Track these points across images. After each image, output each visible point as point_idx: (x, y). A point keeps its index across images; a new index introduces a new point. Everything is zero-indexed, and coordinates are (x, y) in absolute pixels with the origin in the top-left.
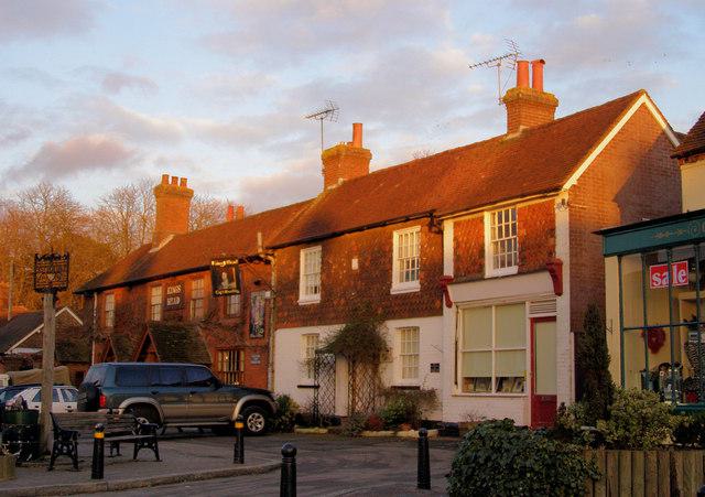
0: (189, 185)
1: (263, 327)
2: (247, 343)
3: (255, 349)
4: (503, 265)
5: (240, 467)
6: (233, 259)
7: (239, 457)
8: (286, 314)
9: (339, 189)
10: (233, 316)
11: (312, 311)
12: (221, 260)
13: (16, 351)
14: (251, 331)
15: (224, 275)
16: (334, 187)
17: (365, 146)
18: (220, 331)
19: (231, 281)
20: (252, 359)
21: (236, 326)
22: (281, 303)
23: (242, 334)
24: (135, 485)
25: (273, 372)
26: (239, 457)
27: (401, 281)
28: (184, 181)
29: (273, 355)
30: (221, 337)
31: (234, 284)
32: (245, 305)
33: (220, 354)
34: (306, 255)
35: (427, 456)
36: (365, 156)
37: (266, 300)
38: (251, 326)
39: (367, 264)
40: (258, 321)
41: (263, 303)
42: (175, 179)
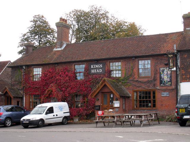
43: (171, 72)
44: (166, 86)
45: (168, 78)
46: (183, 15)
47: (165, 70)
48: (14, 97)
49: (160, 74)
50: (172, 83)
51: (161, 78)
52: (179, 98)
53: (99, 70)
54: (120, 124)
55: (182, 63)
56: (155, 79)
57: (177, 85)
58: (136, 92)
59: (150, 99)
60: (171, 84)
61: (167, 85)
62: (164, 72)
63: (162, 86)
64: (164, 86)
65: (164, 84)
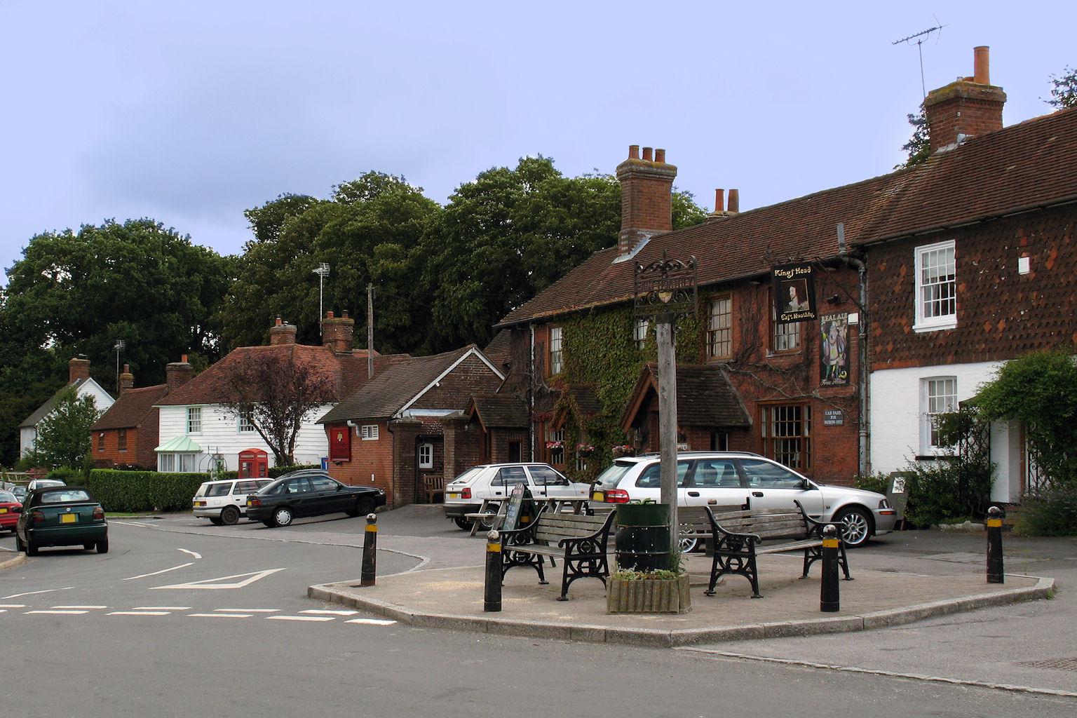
0: (669, 160)
1: (846, 367)
2: (816, 394)
3: (831, 403)
4: (937, 313)
5: (997, 592)
6: (804, 266)
7: (995, 573)
8: (890, 347)
9: (959, 148)
10: (789, 354)
11: (941, 341)
12: (787, 268)
13: (406, 414)
14: (822, 376)
15: (793, 290)
16: (951, 147)
17: (994, 81)
18: (764, 375)
19: (393, 361)
20: (828, 418)
21: (797, 366)
22: (878, 332)
23: (807, 379)
24: (898, 619)
25: (868, 436)
26: (995, 573)
27: (927, 314)
28: (660, 154)
29: (868, 410)
30: (766, 384)
31: (806, 305)
32: (811, 337)
33: (764, 412)
34: (925, 256)
35: (1001, 564)
36: (993, 101)
37: (850, 327)
38: (823, 367)
39: (1049, 265)
40: (835, 356)
41: (843, 333)
42: (647, 151)
43: (849, 329)
44: (835, 385)
45: (841, 355)
46: (40, 232)
47: (834, 324)
48: (249, 384)
49: (822, 341)
50: (852, 376)
51: (822, 354)
52: (281, 469)
53: (624, 240)
54: (318, 487)
55: (874, 297)
56: (808, 362)
57: (861, 379)
58: (767, 407)
59: (800, 419)
60: (848, 379)
61: (836, 381)
62: (832, 333)
63: (825, 386)
64: (831, 386)
65: (830, 379)
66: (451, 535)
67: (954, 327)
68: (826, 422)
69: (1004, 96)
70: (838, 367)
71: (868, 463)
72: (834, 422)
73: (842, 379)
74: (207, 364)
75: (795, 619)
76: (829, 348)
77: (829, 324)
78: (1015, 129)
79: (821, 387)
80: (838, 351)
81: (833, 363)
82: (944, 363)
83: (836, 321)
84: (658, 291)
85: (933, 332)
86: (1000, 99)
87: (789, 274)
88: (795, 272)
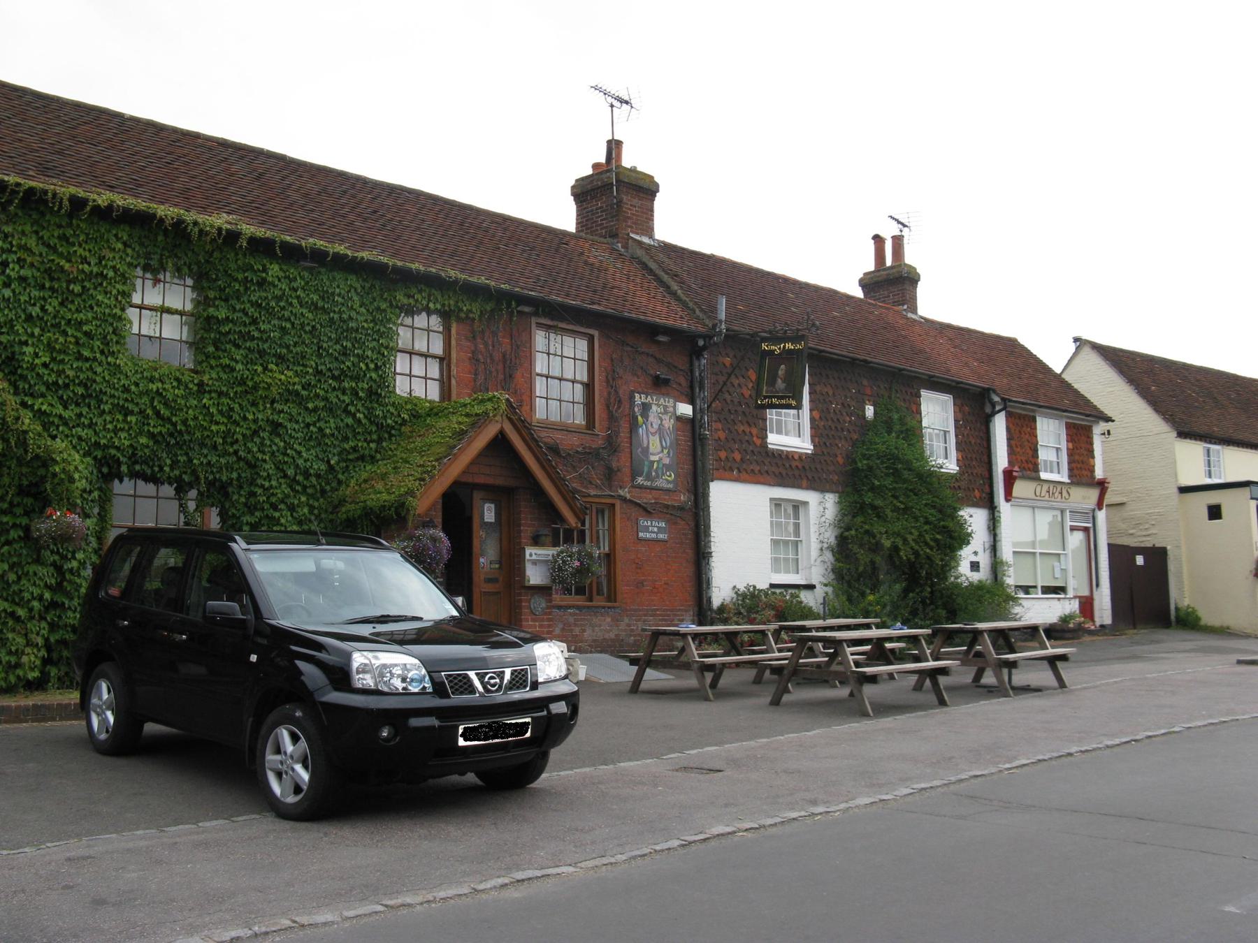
20: (646, 529)
45: (666, 451)
47: (654, 408)
62: (651, 419)
63: (641, 487)
65: (648, 478)
66: (650, 696)
67: (810, 452)
68: (641, 534)
69: (657, 185)
70: (661, 466)
71: (710, 598)
72: (654, 536)
73: (668, 482)
74: (208, 238)
75: (793, 809)
76: (648, 437)
77: (646, 407)
78: (579, 223)
79: (633, 486)
80: (662, 445)
81: (653, 458)
82: (799, 487)
83: (658, 405)
84: (115, 277)
85: (787, 451)
86: (654, 189)
87: (777, 349)
88: (784, 347)
